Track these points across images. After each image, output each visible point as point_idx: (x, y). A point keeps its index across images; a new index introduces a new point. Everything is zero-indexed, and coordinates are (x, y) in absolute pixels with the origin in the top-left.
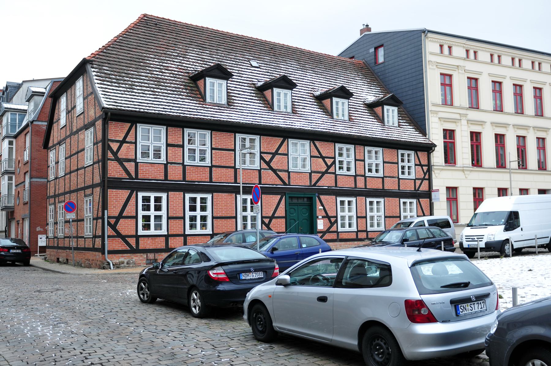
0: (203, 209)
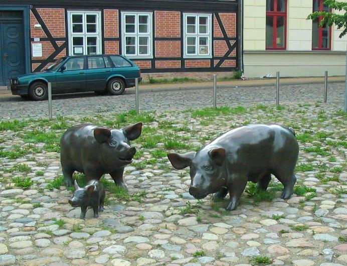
0: (91, 29)
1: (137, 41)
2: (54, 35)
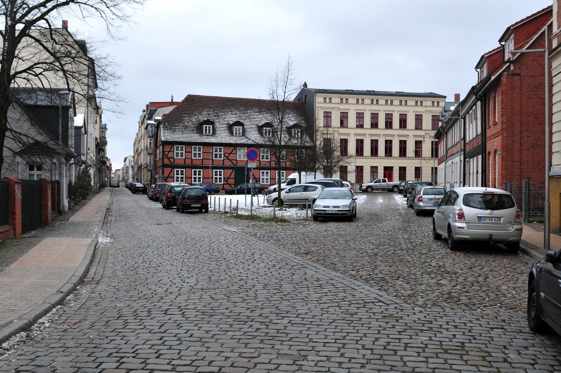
0: (199, 175)
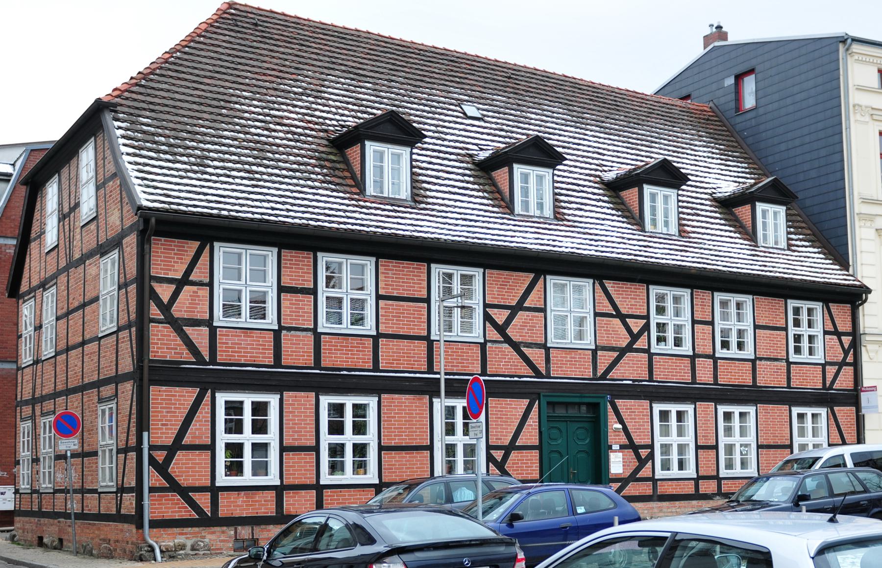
0: (260, 427)
1: (349, 451)
2: (637, 441)
